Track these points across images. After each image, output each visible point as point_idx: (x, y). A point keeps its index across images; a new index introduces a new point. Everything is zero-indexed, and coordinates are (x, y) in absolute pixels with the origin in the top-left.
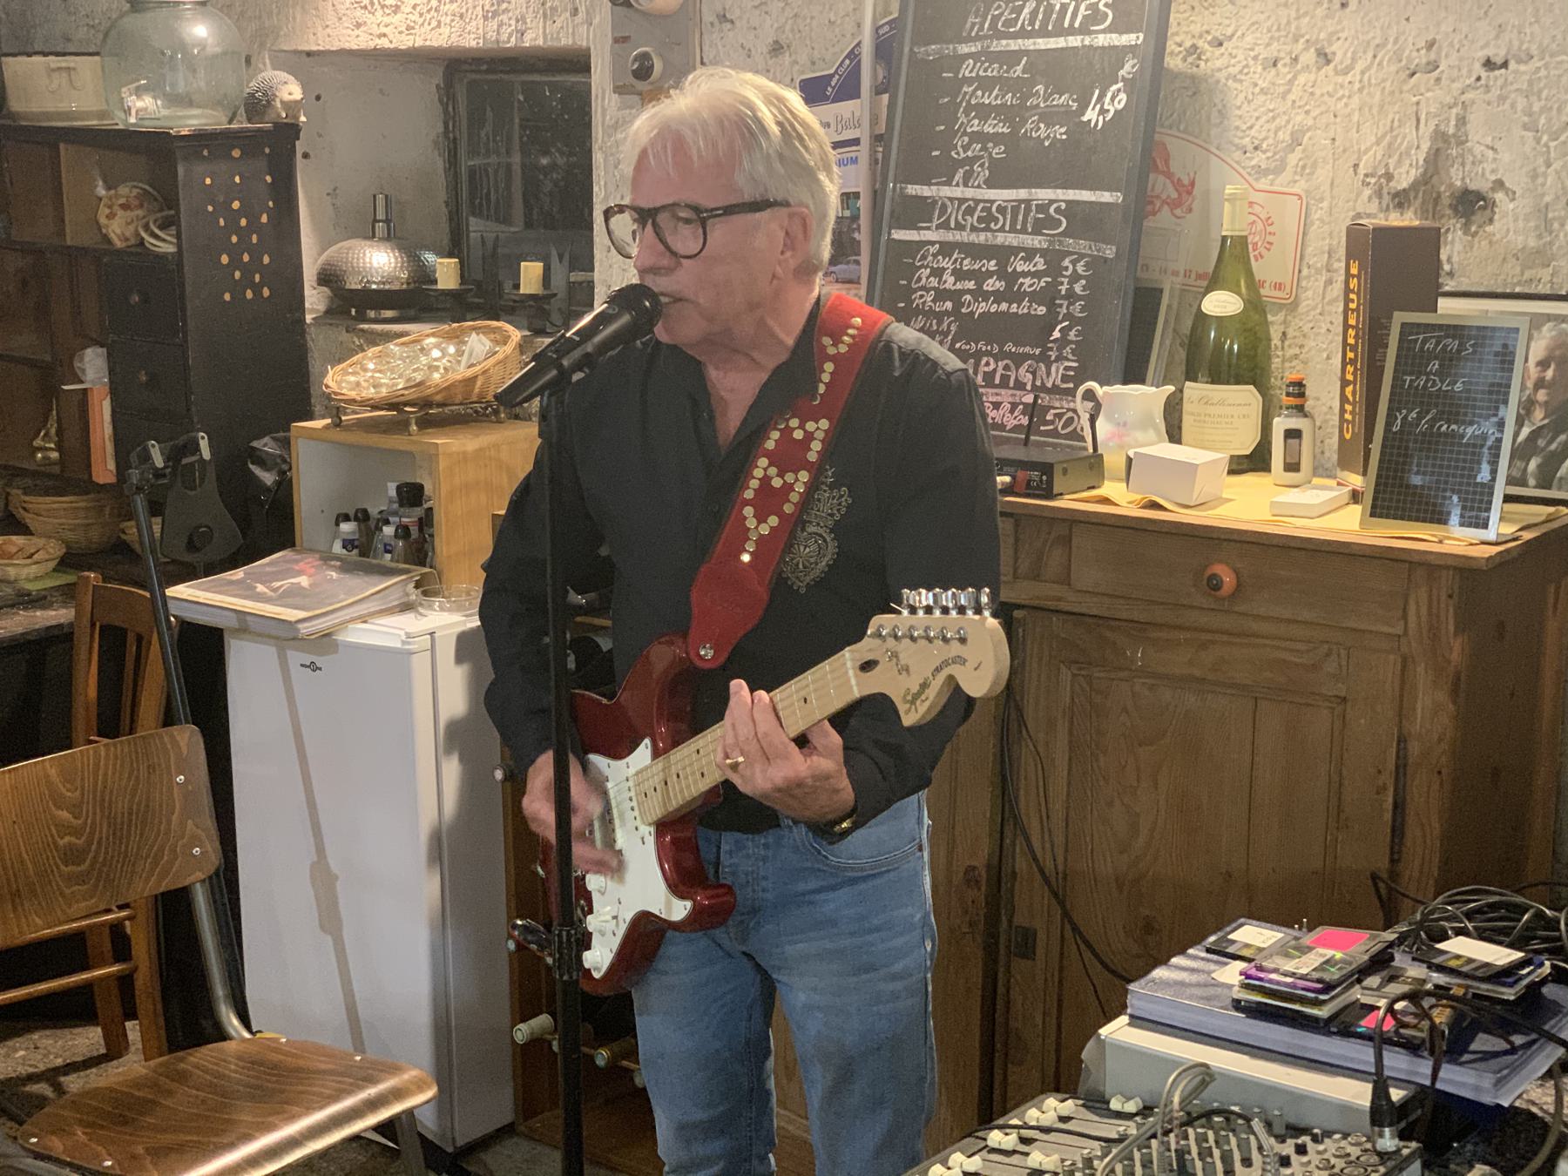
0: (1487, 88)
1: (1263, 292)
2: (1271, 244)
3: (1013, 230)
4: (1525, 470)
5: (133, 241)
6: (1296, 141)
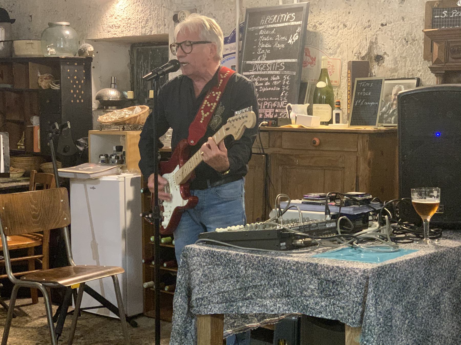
0: (382, 30)
1: (332, 83)
2: (333, 71)
3: (272, 70)
4: (391, 120)
5: (47, 88)
6: (339, 46)
